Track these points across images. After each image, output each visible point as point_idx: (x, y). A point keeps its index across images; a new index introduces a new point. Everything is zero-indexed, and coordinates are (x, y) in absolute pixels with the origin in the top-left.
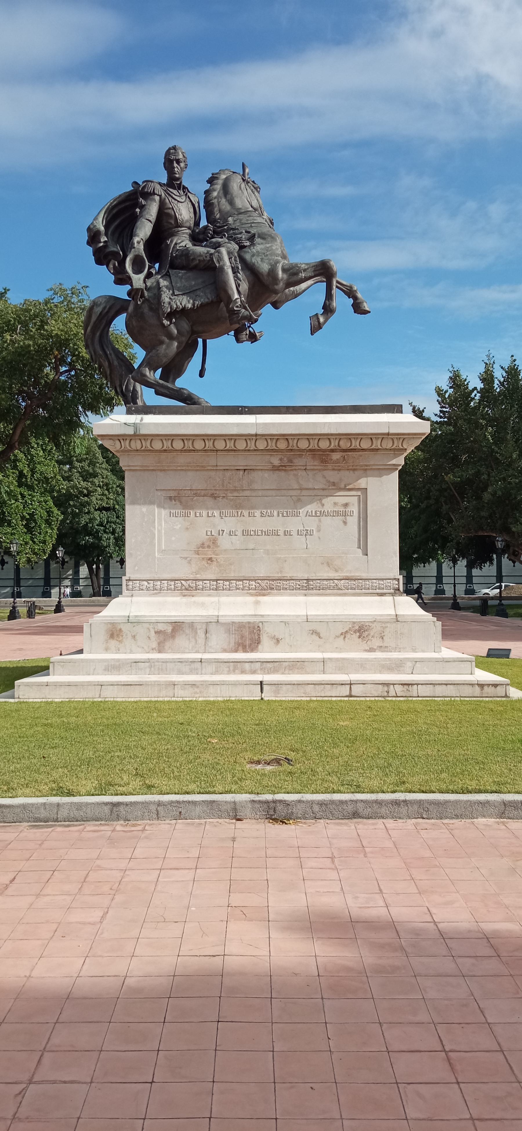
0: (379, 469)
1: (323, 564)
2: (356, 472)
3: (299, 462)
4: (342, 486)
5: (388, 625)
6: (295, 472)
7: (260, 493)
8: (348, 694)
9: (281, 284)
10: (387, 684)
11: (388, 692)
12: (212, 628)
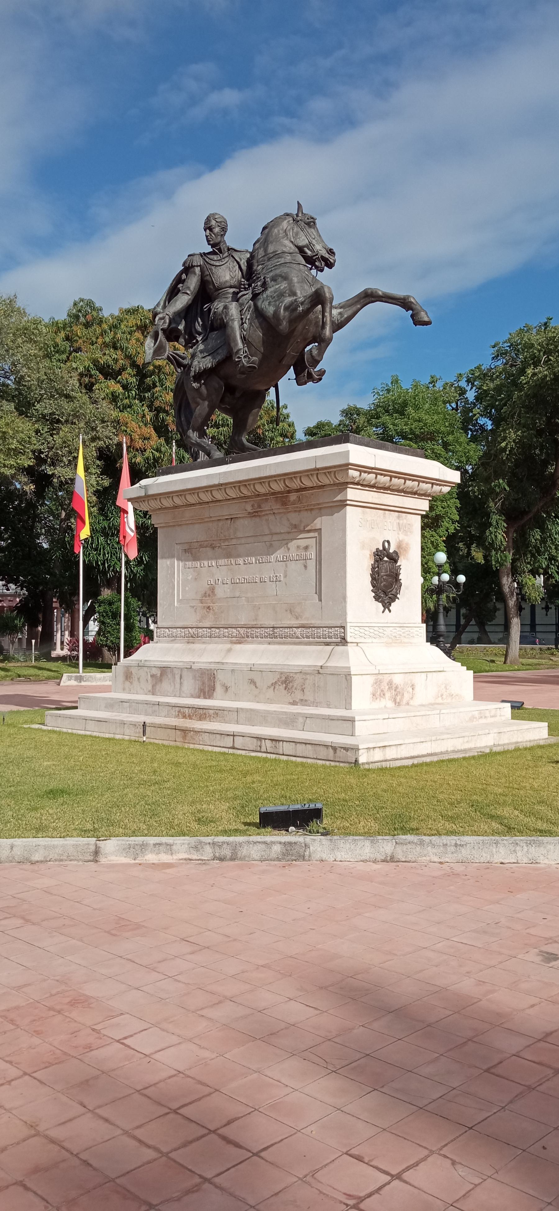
0: (331, 507)
1: (287, 611)
2: (313, 512)
3: (266, 507)
4: (302, 528)
5: (308, 677)
6: (266, 517)
7: (243, 541)
8: (231, 745)
9: (285, 323)
10: (259, 738)
11: (260, 747)
12: (185, 673)
